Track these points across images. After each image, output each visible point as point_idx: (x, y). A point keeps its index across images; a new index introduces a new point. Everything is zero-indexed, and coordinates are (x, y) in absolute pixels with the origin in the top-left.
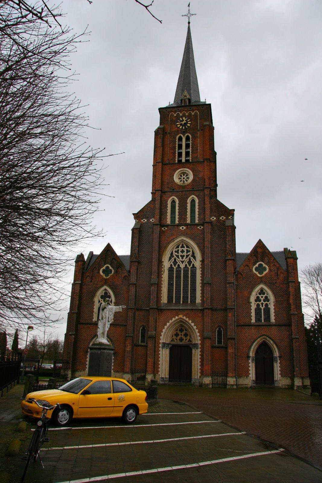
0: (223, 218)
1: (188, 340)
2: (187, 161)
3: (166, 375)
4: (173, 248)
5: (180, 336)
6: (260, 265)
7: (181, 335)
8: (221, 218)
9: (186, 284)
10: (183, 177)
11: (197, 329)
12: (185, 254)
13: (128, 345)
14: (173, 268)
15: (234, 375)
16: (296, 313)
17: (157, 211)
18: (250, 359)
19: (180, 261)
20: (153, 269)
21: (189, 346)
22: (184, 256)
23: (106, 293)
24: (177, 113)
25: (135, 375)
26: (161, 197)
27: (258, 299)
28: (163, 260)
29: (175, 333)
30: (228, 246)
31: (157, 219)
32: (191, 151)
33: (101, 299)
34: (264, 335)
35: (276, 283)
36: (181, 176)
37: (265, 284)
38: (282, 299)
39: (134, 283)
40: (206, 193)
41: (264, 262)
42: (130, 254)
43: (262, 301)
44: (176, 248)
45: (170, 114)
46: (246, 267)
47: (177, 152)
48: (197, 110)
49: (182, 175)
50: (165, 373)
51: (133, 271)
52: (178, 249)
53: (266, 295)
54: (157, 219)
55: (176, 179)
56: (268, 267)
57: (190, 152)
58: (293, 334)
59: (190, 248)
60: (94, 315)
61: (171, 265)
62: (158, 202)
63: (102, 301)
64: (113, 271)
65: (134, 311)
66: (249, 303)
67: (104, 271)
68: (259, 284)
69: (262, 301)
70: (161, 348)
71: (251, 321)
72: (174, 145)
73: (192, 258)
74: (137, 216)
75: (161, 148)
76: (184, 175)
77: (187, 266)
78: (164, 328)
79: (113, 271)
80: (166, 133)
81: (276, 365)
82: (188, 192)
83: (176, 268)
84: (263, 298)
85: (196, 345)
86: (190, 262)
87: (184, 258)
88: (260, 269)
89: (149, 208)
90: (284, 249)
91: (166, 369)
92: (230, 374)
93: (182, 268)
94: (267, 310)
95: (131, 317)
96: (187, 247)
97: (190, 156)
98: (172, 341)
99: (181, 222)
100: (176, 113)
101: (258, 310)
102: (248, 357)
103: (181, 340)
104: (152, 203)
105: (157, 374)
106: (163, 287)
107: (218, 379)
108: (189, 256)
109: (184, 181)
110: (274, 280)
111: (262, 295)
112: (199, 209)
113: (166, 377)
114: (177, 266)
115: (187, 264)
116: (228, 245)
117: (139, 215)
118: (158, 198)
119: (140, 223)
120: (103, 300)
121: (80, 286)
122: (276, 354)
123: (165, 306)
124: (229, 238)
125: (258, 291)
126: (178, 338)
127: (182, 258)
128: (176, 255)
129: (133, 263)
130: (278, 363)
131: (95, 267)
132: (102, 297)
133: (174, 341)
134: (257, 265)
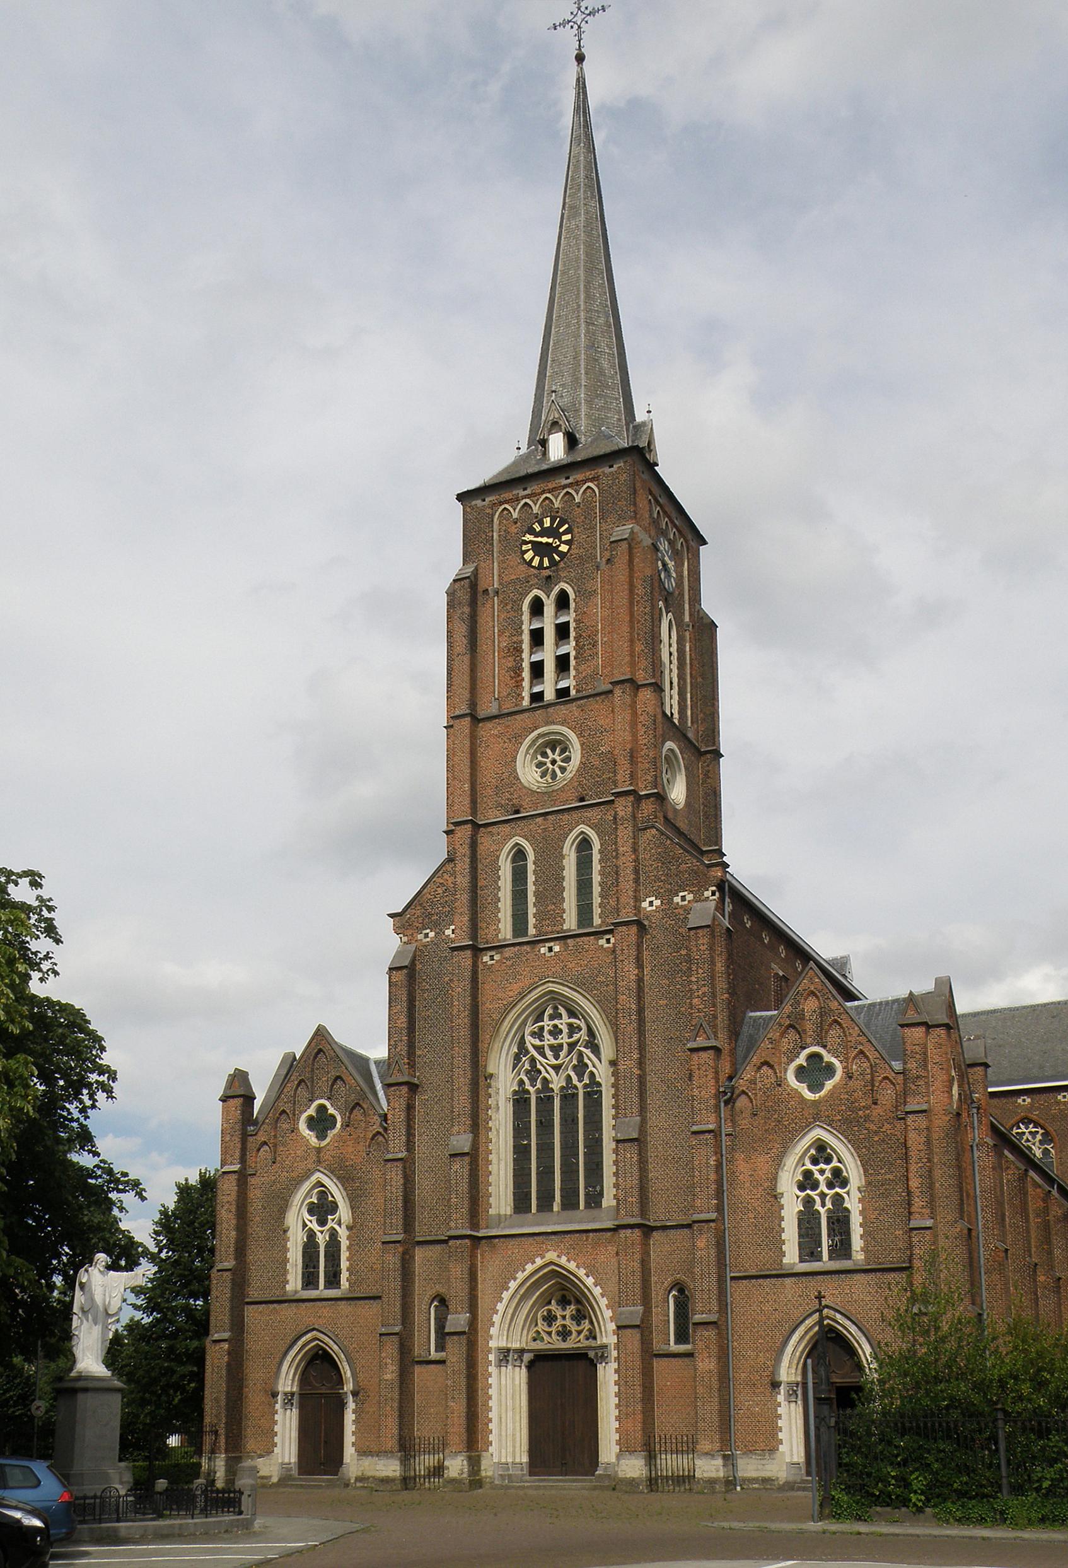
1: (585, 1332)
2: (563, 693)
3: (518, 1455)
4: (524, 1023)
5: (559, 1322)
6: (815, 1057)
7: (564, 1317)
8: (677, 899)
9: (569, 1148)
11: (603, 1296)
12: (564, 1039)
13: (386, 1364)
18: (782, 1391)
19: (548, 1068)
20: (455, 1103)
26: (474, 845)
27: (807, 1182)
32: (573, 654)
33: (310, 1218)
35: (867, 1118)
36: (544, 755)
38: (888, 1177)
39: (400, 1156)
40: (621, 814)
41: (824, 1047)
42: (386, 1055)
43: (823, 1187)
49: (549, 751)
57: (572, 658)
60: (290, 1271)
63: (311, 1221)
65: (401, 1249)
66: (775, 1197)
68: (807, 1127)
69: (823, 1187)
70: (495, 1366)
71: (782, 1261)
72: (515, 639)
74: (402, 920)
75: (467, 659)
76: (553, 751)
77: (572, 1083)
79: (339, 1118)
80: (486, 591)
82: (566, 816)
87: (562, 1054)
88: (815, 1071)
89: (440, 891)
92: (703, 1442)
94: (840, 1221)
96: (572, 1014)
101: (808, 1220)
103: (564, 1334)
105: (484, 1454)
107: (680, 1461)
116: (698, 997)
117: (409, 918)
121: (238, 1180)
124: (700, 971)
126: (553, 1329)
128: (535, 1047)
133: (542, 1339)
134: (801, 1060)
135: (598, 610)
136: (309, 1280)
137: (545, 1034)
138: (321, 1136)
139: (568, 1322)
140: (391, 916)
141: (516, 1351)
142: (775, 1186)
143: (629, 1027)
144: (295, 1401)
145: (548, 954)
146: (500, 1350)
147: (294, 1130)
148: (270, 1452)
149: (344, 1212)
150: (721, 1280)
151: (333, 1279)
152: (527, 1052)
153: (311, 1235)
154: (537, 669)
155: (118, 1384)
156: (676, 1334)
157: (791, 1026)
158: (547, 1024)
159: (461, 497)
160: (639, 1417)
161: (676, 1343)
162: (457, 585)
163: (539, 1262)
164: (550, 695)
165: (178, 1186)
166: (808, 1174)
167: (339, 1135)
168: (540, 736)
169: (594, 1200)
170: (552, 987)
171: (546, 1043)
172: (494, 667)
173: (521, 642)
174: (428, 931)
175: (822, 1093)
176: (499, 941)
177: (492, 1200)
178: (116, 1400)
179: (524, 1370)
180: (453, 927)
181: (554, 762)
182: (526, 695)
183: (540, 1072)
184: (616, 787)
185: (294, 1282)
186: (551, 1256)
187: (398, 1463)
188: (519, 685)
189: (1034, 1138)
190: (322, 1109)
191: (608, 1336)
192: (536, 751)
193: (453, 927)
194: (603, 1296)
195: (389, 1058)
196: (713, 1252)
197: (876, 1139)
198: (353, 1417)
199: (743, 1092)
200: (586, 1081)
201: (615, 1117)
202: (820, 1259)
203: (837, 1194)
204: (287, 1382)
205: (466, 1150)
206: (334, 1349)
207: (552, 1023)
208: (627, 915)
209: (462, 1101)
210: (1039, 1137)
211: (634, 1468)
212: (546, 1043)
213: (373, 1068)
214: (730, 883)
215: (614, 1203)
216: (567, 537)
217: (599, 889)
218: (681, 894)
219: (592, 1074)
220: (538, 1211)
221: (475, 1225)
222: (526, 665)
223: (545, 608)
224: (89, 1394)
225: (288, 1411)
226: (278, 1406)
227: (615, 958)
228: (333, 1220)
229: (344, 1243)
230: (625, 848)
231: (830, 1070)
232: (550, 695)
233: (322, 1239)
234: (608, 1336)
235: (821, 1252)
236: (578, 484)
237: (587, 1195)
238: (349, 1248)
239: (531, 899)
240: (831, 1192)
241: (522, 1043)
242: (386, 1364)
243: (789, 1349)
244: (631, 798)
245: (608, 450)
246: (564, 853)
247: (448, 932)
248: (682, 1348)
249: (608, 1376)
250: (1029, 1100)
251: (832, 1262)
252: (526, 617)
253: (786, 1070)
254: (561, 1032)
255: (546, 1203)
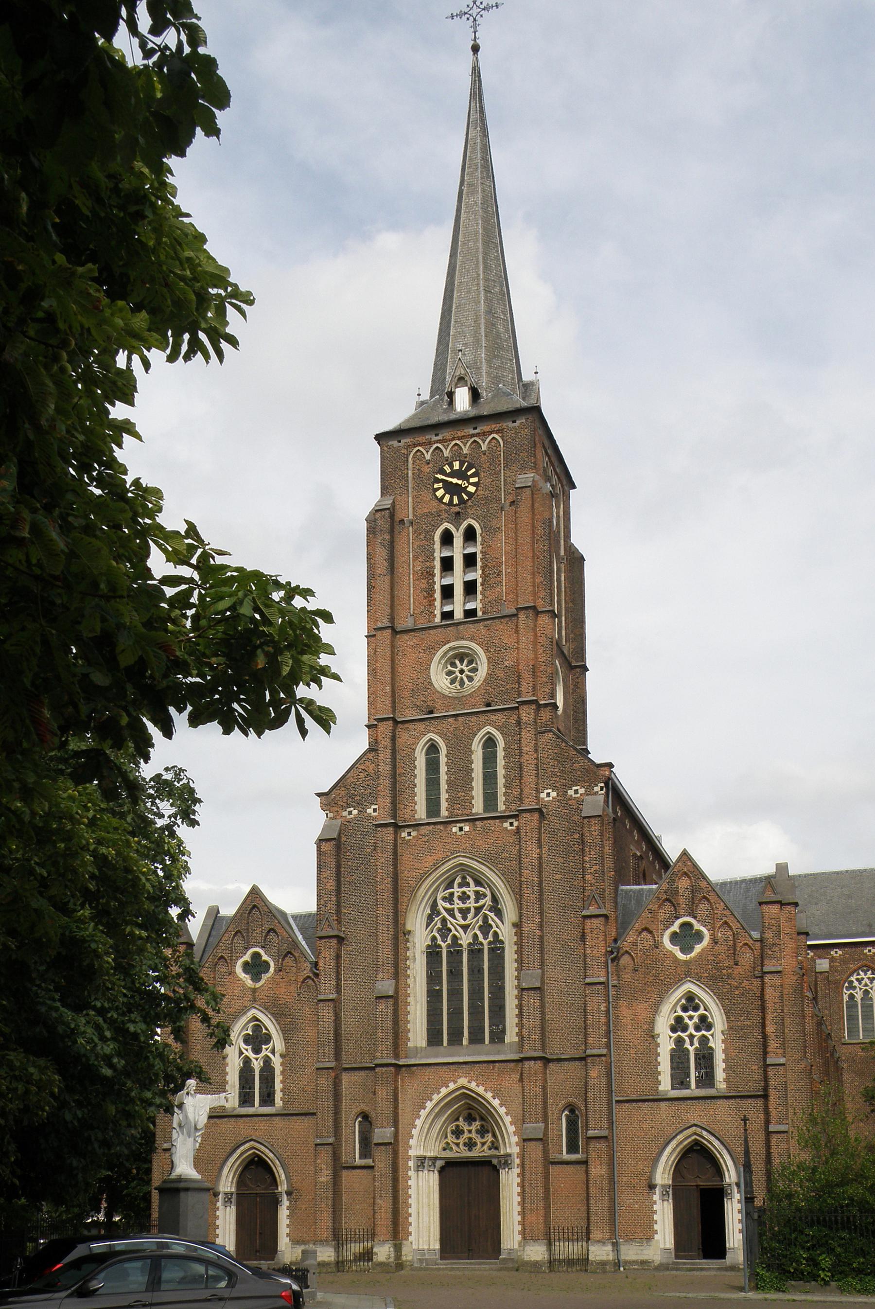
0: (576, 792)
1: (488, 1144)
3: (432, 1243)
4: (437, 890)
5: (466, 1135)
7: (470, 1132)
8: (571, 792)
10: (457, 670)
12: (471, 904)
13: (321, 1169)
14: (440, 946)
15: (607, 1236)
16: (782, 1060)
17: (385, 783)
18: (657, 1192)
19: (458, 927)
21: (491, 1162)
22: (468, 910)
23: (257, 1028)
24: (435, 446)
25: (349, 1246)
27: (679, 1025)
28: (409, 927)
29: (452, 1127)
30: (588, 877)
31: (384, 808)
32: (479, 581)
33: (246, 1047)
34: (695, 1125)
35: (729, 976)
36: (453, 665)
37: (699, 979)
38: (746, 1023)
39: (331, 997)
41: (695, 918)
43: (691, 1030)
44: (446, 889)
45: (412, 454)
46: (645, 933)
47: (437, 587)
48: (497, 432)
49: (457, 662)
50: (429, 1236)
51: (327, 963)
52: (452, 890)
53: (702, 1011)
54: (384, 808)
55: (440, 681)
56: (708, 930)
57: (479, 584)
58: (773, 1121)
59: (484, 888)
61: (434, 939)
62: (385, 755)
63: (247, 1050)
64: (272, 964)
65: (333, 1074)
66: (652, 1036)
67: (246, 967)
68: (679, 981)
69: (691, 1030)
72: (428, 564)
73: (492, 914)
75: (387, 579)
78: (419, 1117)
79: (272, 964)
80: (402, 521)
81: (730, 1208)
83: (449, 946)
84: (693, 1021)
85: (506, 1160)
86: (486, 928)
87: (470, 916)
89: (362, 775)
90: (778, 866)
91: (429, 1227)
93: (465, 945)
94: (705, 1058)
95: (328, 1092)
96: (478, 883)
97: (479, 597)
98: (444, 1149)
99: (456, 811)
100: (431, 450)
101: (679, 1056)
102: (652, 1187)
104: (370, 756)
106: (412, 1003)
108: (483, 911)
109: (462, 683)
110: (724, 969)
111: (691, 1013)
112: (506, 768)
113: (432, 1247)
114: (449, 941)
115: (478, 933)
117: (335, 798)
118: (385, 742)
119: (338, 822)
120: (249, 1048)
122: (730, 1177)
123: (419, 1055)
125: (680, 1000)
127: (465, 918)
128: (446, 909)
129: (323, 941)
130: (735, 1200)
131: (222, 957)
132: (247, 1040)
134: (675, 928)
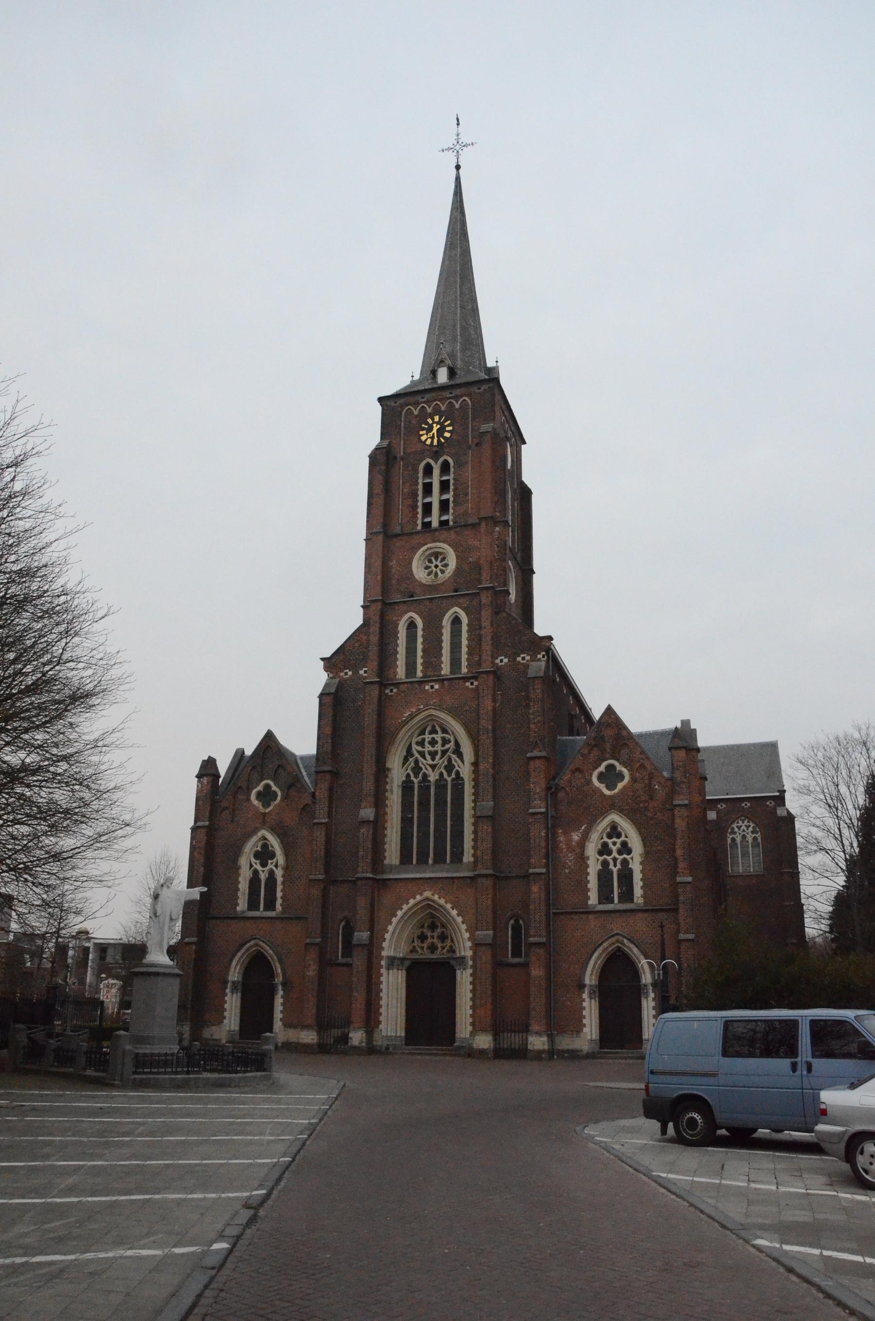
4: (411, 736)
5: (429, 940)
6: (610, 767)
8: (519, 659)
12: (438, 747)
26: (382, 616)
27: (604, 850)
32: (451, 499)
33: (255, 861)
36: (430, 561)
39: (324, 821)
40: (484, 601)
41: (618, 760)
43: (615, 854)
60: (240, 897)
63: (256, 864)
68: (604, 813)
69: (615, 854)
74: (330, 663)
76: (436, 559)
79: (279, 793)
80: (395, 457)
87: (438, 757)
88: (610, 777)
89: (357, 644)
94: (626, 876)
96: (445, 731)
101: (604, 875)
116: (534, 723)
126: (425, 945)
133: (417, 952)
134: (602, 768)
135: (469, 474)
136: (253, 904)
137: (426, 743)
138: (266, 805)
139: (435, 940)
140: (322, 659)
141: (399, 959)
142: (584, 851)
143: (486, 740)
144: (240, 987)
145: (431, 690)
146: (389, 958)
147: (248, 800)
148: (221, 1022)
149: (280, 858)
150: (548, 914)
151: (270, 904)
152: (412, 755)
153: (256, 872)
154: (428, 508)
155: (177, 971)
156: (512, 950)
157: (595, 745)
158: (428, 737)
159: (381, 400)
160: (489, 1007)
161: (512, 957)
162: (378, 452)
163: (419, 898)
164: (435, 524)
165: (686, 723)
166: (605, 845)
167: (279, 805)
168: (428, 549)
169: (457, 857)
170: (433, 712)
171: (426, 750)
172: (400, 505)
173: (418, 490)
174: (347, 671)
175: (616, 791)
176: (397, 680)
177: (386, 854)
178: (176, 982)
179: (404, 972)
180: (366, 669)
181: (436, 566)
182: (419, 522)
183: (421, 769)
184: (480, 584)
185: (242, 905)
186: (427, 894)
187: (315, 1034)
188: (415, 516)
189: (747, 829)
190: (267, 787)
191: (465, 949)
192: (425, 559)
193: (366, 669)
194: (463, 923)
195: (317, 754)
196: (543, 895)
197: (651, 822)
198: (281, 1000)
199: (563, 788)
200: (453, 776)
201: (475, 801)
202: (612, 902)
203: (625, 859)
204: (235, 974)
205: (371, 819)
206: (269, 952)
207: (431, 736)
208: (486, 667)
209: (369, 785)
210: (751, 829)
211: (484, 1041)
212: (426, 750)
213: (299, 762)
214: (553, 651)
215: (472, 859)
216: (450, 428)
217: (466, 649)
218: (522, 656)
219: (458, 773)
220: (417, 863)
221: (374, 870)
222: (420, 504)
223: (434, 470)
224: (160, 978)
225: (235, 995)
226: (228, 991)
227: (479, 694)
228: (272, 863)
229: (279, 879)
230: (486, 623)
231: (621, 777)
232: (435, 524)
233: (263, 877)
234: (465, 949)
235: (613, 897)
236: (457, 398)
237: (452, 853)
238: (283, 883)
239: (420, 653)
240: (621, 857)
241: (409, 748)
242: (309, 965)
243: (592, 962)
244: (490, 592)
245: (473, 380)
246: (443, 624)
247: (361, 672)
248: (517, 960)
249: (464, 980)
250: (724, 806)
251: (621, 904)
252: (421, 475)
253: (591, 775)
254: (437, 742)
255: (423, 859)
